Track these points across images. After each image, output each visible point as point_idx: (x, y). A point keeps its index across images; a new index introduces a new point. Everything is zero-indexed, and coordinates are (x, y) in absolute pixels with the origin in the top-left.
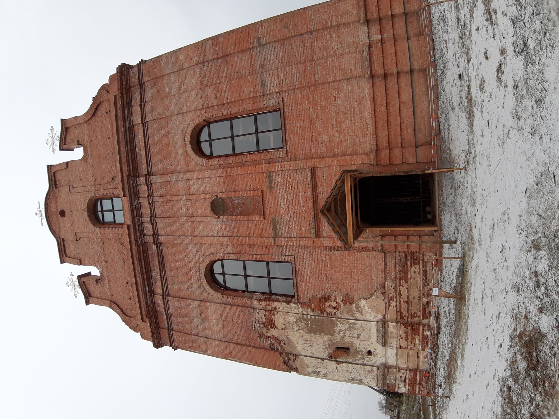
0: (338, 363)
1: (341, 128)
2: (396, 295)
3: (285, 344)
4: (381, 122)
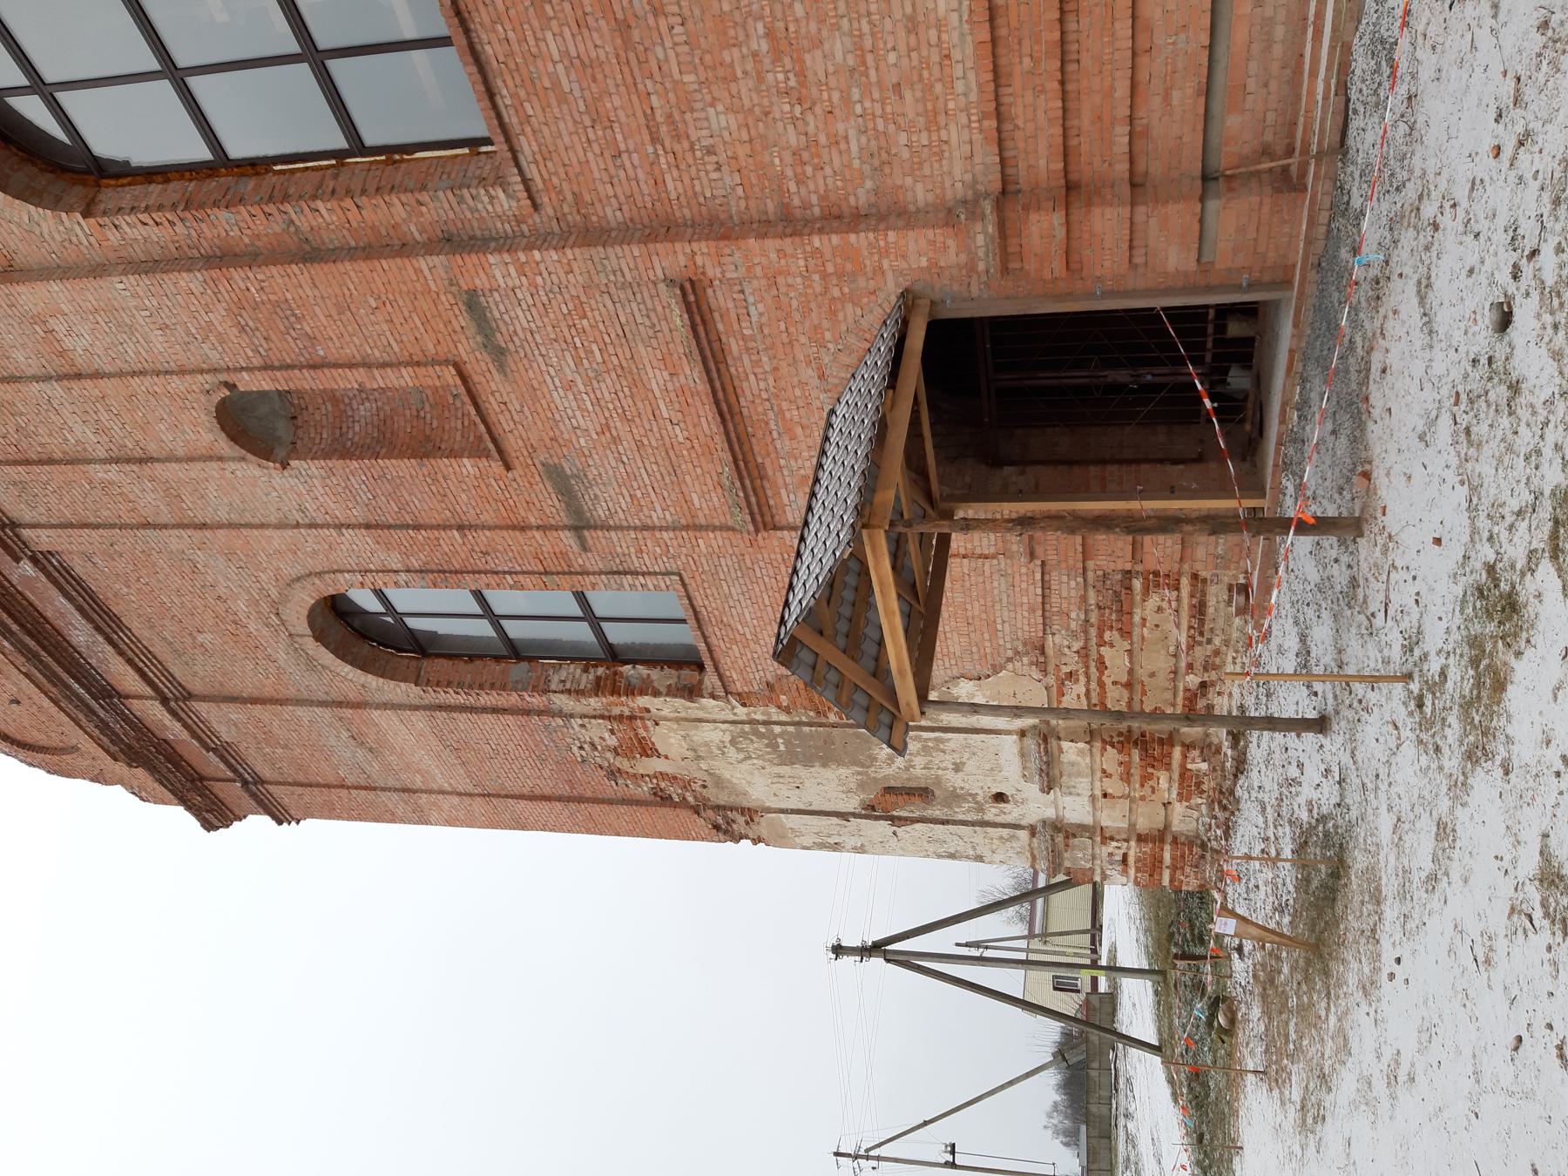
0: (896, 821)
1: (801, 74)
2: (1087, 667)
3: (704, 787)
4: (1026, 50)
